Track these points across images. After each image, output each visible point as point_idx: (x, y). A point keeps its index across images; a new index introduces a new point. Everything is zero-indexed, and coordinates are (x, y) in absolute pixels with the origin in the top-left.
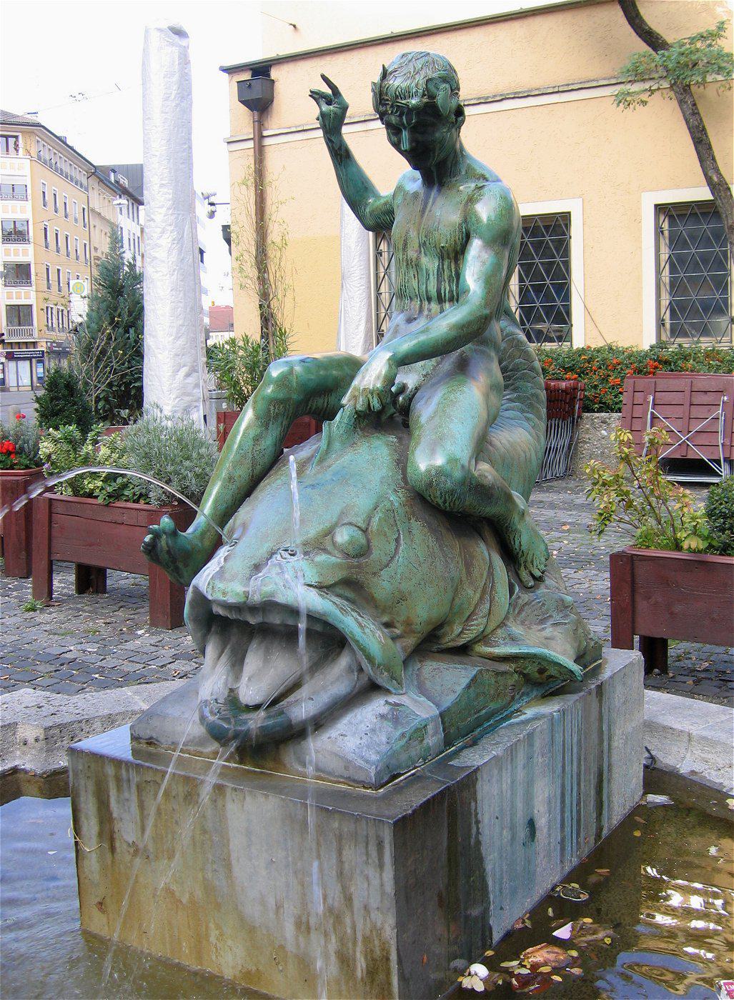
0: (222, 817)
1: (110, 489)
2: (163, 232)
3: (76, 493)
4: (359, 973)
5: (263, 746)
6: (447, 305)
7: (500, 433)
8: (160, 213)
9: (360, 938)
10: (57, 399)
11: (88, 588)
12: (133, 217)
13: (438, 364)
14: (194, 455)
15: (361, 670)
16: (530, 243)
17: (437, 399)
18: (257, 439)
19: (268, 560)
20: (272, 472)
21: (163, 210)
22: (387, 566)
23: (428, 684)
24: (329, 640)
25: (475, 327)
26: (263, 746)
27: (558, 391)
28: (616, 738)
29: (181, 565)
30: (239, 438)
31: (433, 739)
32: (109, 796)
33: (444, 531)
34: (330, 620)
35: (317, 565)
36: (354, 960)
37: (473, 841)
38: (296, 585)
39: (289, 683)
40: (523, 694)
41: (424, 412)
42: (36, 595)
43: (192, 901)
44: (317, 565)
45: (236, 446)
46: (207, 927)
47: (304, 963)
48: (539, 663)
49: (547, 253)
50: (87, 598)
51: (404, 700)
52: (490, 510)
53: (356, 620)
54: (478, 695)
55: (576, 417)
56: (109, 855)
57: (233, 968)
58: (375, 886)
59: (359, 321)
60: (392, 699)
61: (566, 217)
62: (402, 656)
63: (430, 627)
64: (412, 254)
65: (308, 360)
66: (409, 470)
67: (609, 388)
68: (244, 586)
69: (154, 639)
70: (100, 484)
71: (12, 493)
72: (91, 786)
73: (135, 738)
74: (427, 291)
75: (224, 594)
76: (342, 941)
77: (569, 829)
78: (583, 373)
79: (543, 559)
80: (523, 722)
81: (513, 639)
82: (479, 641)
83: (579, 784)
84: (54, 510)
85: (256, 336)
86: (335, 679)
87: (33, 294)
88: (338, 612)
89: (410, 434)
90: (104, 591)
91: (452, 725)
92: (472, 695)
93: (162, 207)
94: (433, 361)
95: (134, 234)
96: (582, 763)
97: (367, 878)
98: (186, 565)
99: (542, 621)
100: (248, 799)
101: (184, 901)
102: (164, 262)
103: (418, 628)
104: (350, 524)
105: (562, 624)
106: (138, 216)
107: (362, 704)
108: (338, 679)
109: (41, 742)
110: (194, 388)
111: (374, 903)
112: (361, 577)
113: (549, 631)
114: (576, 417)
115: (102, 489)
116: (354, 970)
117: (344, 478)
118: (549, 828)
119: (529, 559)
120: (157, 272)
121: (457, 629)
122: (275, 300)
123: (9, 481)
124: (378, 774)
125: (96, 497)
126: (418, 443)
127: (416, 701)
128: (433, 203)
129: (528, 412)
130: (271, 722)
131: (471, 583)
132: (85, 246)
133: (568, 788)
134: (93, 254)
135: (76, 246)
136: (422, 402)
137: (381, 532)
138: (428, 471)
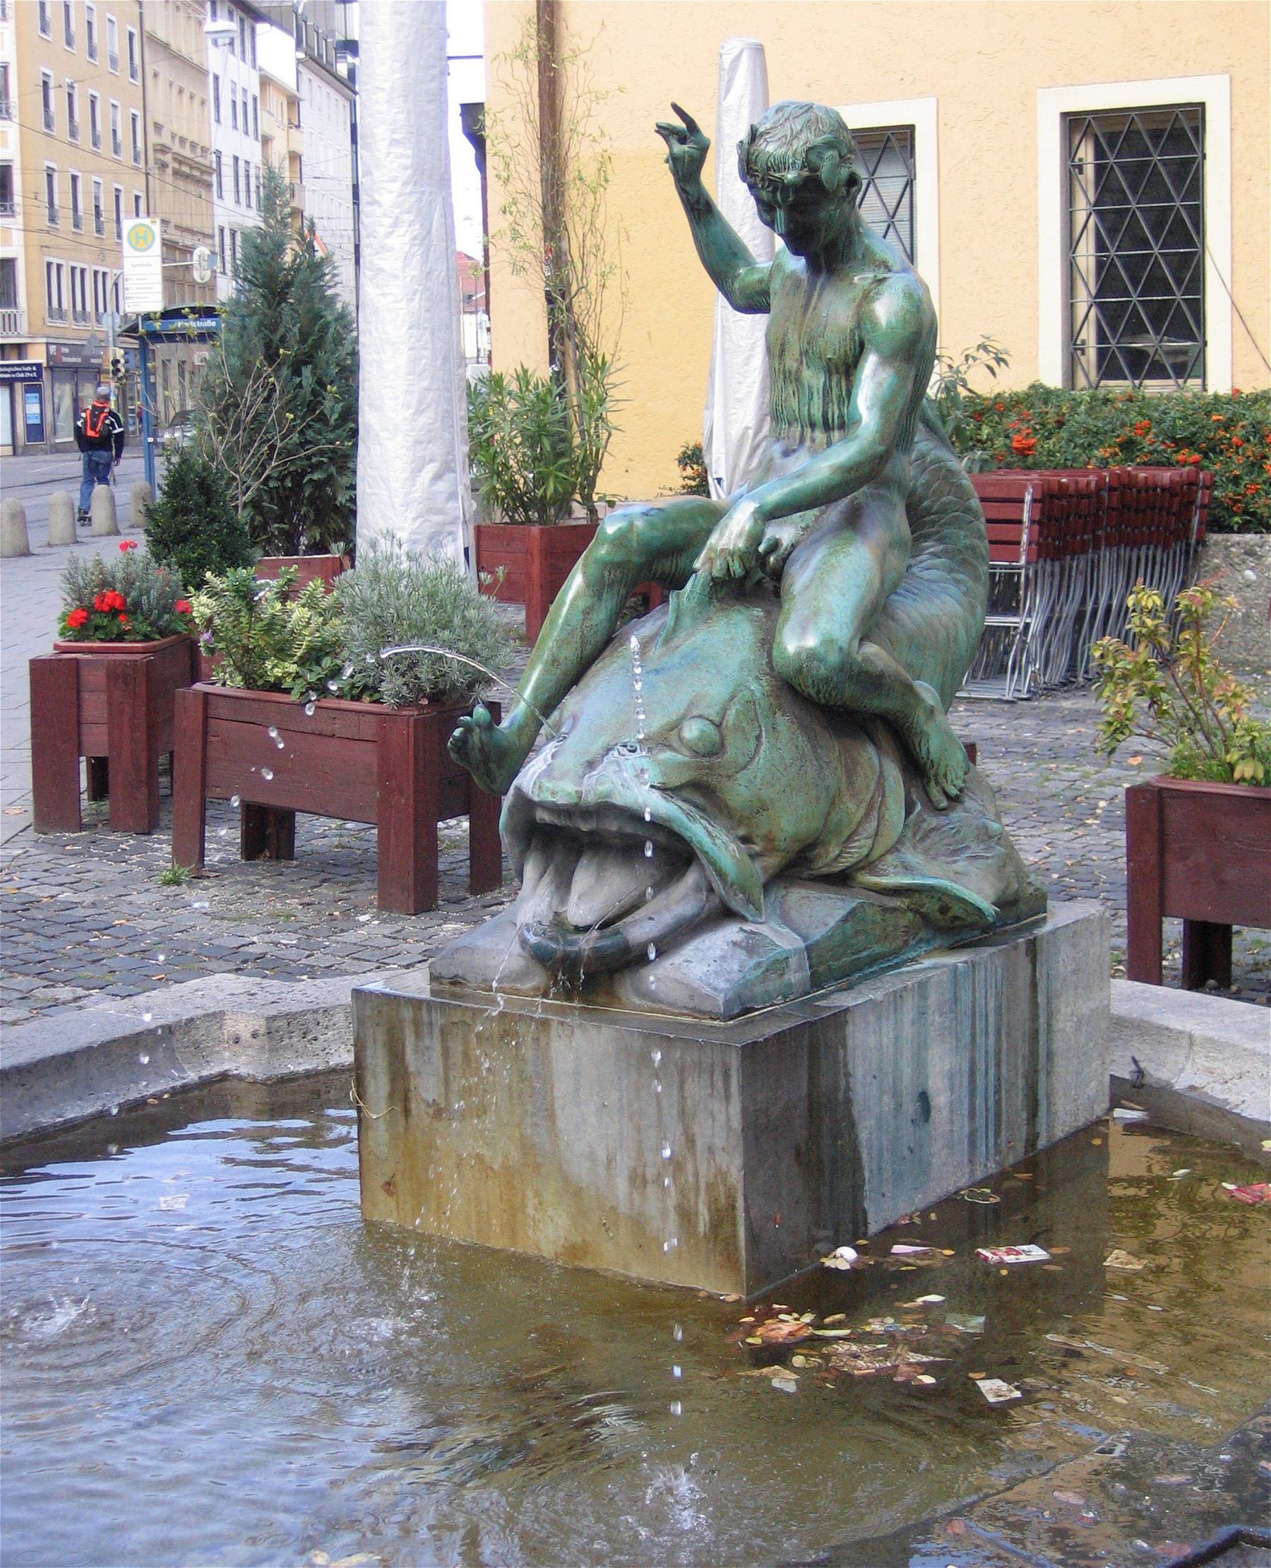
0: (544, 1059)
1: (311, 678)
2: (395, 225)
3: (249, 682)
4: (701, 1229)
5: (591, 974)
6: (836, 434)
7: (910, 602)
8: (390, 192)
9: (703, 1185)
10: (186, 511)
11: (261, 851)
12: (243, 52)
13: (822, 513)
14: (457, 621)
15: (711, 890)
16: (1120, 168)
17: (815, 561)
18: (587, 612)
19: (603, 756)
20: (606, 653)
21: (396, 186)
22: (745, 767)
23: (794, 915)
24: (677, 855)
25: (867, 469)
26: (591, 974)
27: (1155, 489)
28: (1061, 1018)
29: (493, 766)
30: (565, 610)
31: (796, 976)
32: (404, 1045)
33: (818, 728)
34: (675, 828)
35: (660, 763)
36: (696, 1214)
37: (841, 1095)
38: (637, 785)
39: (626, 901)
40: (921, 940)
41: (799, 579)
42: (179, 855)
43: (505, 1166)
44: (660, 763)
45: (561, 621)
46: (524, 1196)
47: (638, 1223)
48: (940, 899)
49: (1155, 189)
50: (261, 866)
51: (763, 929)
52: (878, 703)
53: (705, 828)
54: (857, 933)
55: (1193, 541)
56: (402, 1122)
57: (554, 1242)
58: (721, 1122)
59: (752, 349)
60: (747, 927)
61: (1195, 114)
62: (762, 879)
63: (796, 847)
64: (791, 363)
65: (653, 512)
66: (775, 653)
67: (1264, 482)
68: (576, 785)
69: (389, 929)
70: (293, 668)
71: (126, 684)
72: (381, 1037)
73: (435, 978)
74: (809, 414)
75: (553, 793)
76: (682, 1193)
77: (983, 1122)
78: (1212, 449)
79: (961, 773)
80: (915, 971)
81: (907, 869)
82: (863, 868)
83: (998, 1065)
84: (211, 713)
85: (542, 371)
86: (681, 900)
87: (17, 237)
88: (684, 817)
89: (780, 606)
90: (291, 856)
91: (821, 962)
92: (849, 932)
93: (394, 180)
94: (816, 511)
95: (245, 91)
96: (1003, 1038)
97: (712, 1114)
98: (500, 767)
99: (955, 852)
100: (577, 1032)
101: (496, 1167)
102: (396, 277)
103: (783, 845)
104: (700, 716)
105: (983, 857)
106: (254, 48)
107: (712, 930)
108: (684, 898)
109: (261, 1038)
110: (448, 500)
111: (719, 1142)
112: (713, 781)
113: (961, 865)
114: (1193, 541)
115: (298, 676)
116: (696, 1226)
117: (693, 662)
118: (951, 1111)
119: (942, 772)
120: (383, 295)
121: (834, 851)
122: (582, 297)
123: (121, 662)
124: (728, 1002)
125: (288, 691)
126: (787, 619)
127: (776, 931)
128: (820, 295)
129: (959, 571)
130: (607, 942)
131: (853, 796)
132: (134, 120)
133: (981, 1066)
134: (153, 139)
135: (114, 123)
136: (798, 565)
137: (737, 728)
138: (798, 654)
